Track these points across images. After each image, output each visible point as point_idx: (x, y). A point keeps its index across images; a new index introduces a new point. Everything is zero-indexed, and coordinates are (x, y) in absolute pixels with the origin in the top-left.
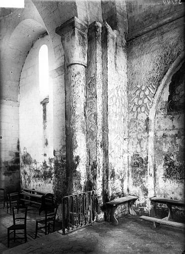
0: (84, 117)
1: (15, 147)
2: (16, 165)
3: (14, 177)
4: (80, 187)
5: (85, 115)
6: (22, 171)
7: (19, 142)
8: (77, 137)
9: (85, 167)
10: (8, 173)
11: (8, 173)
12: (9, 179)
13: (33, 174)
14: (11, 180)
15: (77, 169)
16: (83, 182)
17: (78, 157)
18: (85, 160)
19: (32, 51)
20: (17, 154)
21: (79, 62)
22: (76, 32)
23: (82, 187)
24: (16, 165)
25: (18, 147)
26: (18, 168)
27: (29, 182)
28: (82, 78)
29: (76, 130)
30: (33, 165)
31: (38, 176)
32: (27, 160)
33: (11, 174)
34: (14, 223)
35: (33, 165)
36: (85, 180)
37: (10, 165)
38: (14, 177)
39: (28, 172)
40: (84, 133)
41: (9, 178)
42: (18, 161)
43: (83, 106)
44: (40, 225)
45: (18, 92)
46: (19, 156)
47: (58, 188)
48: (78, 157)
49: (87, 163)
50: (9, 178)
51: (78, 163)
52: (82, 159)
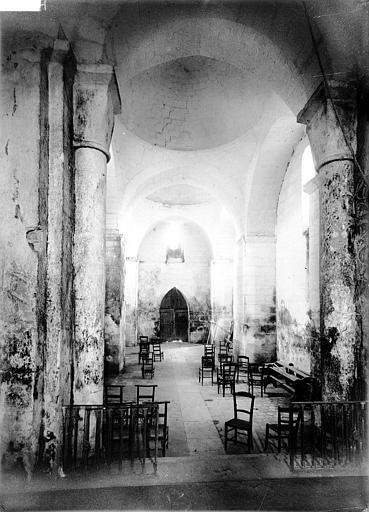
0: (348, 255)
1: (271, 298)
2: (271, 324)
3: (267, 341)
4: (339, 388)
5: (351, 250)
6: (278, 332)
7: (275, 293)
8: (332, 292)
9: (350, 350)
10: (259, 335)
11: (259, 335)
12: (261, 343)
13: (292, 341)
14: (263, 345)
15: (333, 353)
16: (344, 379)
17: (335, 329)
18: (353, 336)
19: (293, 161)
20: (273, 310)
21: (336, 155)
22: (255, 160)
23: (344, 388)
24: (271, 324)
25: (274, 300)
26: (274, 328)
27: (288, 352)
28: (345, 183)
29: (331, 280)
30: (293, 327)
31: (299, 345)
32: (286, 322)
33: (263, 336)
34: (236, 415)
35: (293, 327)
36: (350, 375)
37: (263, 324)
38: (267, 341)
39: (286, 336)
40: (349, 284)
41: (260, 342)
42: (273, 319)
43: (345, 234)
44: (271, 432)
45: (275, 223)
46: (274, 312)
47: (316, 375)
48: (335, 329)
49: (357, 342)
50: (260, 342)
51: (334, 341)
52: (343, 334)
